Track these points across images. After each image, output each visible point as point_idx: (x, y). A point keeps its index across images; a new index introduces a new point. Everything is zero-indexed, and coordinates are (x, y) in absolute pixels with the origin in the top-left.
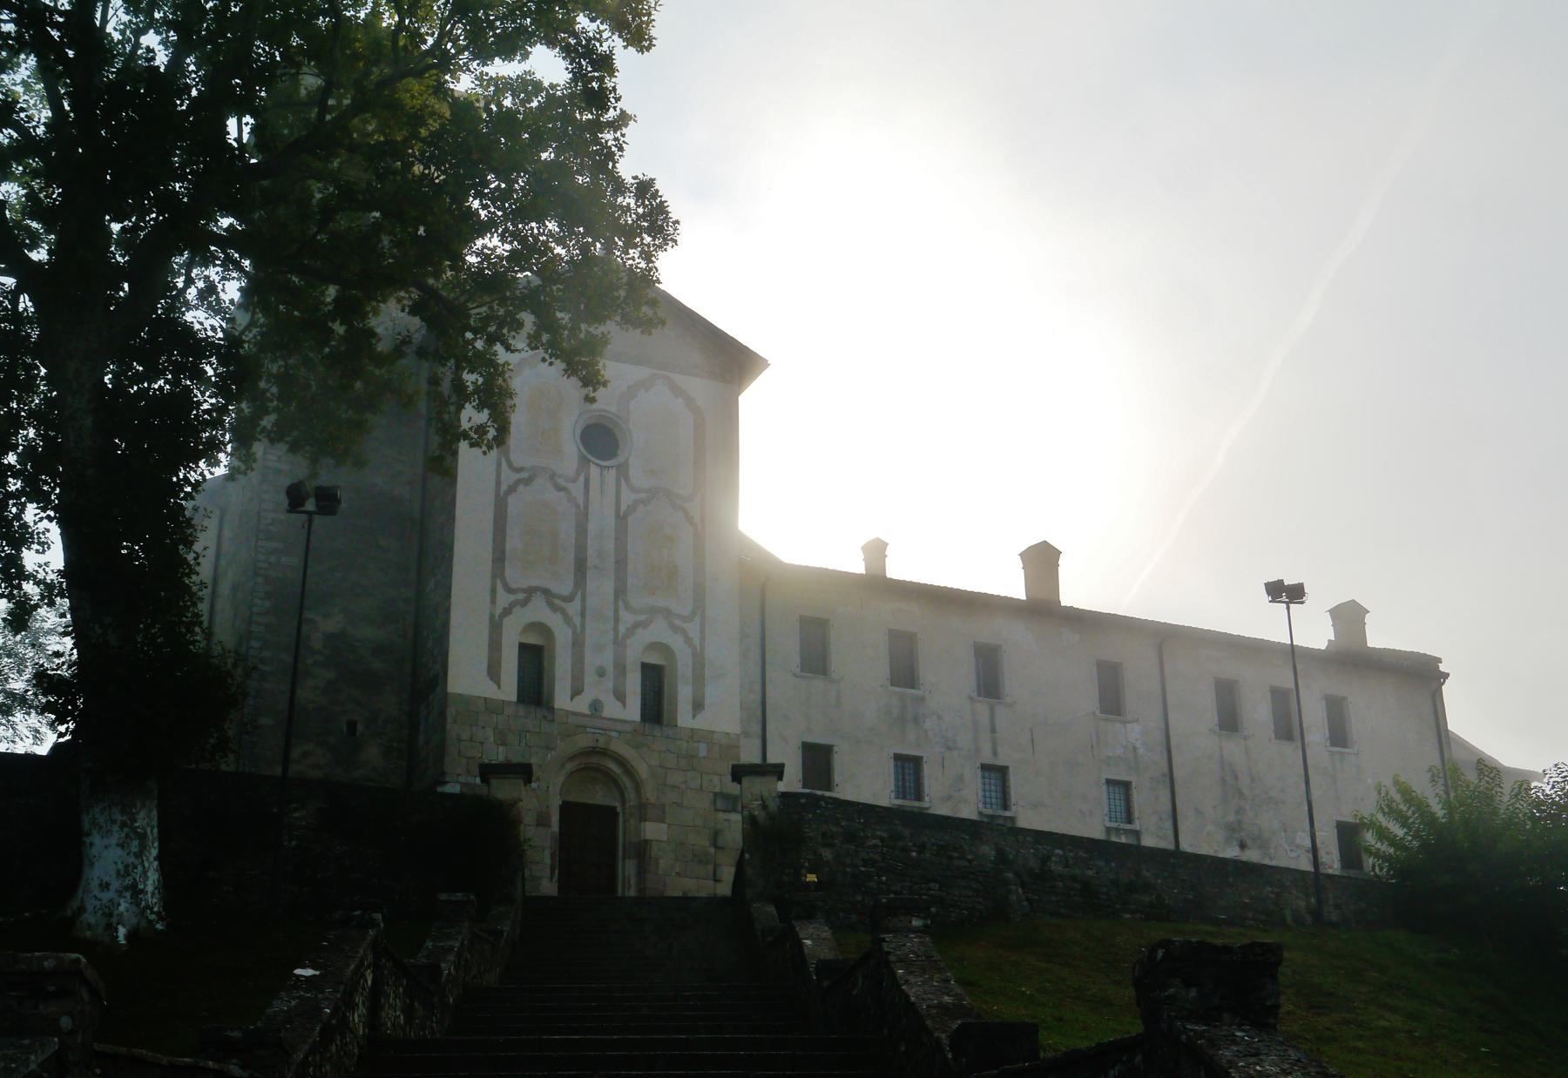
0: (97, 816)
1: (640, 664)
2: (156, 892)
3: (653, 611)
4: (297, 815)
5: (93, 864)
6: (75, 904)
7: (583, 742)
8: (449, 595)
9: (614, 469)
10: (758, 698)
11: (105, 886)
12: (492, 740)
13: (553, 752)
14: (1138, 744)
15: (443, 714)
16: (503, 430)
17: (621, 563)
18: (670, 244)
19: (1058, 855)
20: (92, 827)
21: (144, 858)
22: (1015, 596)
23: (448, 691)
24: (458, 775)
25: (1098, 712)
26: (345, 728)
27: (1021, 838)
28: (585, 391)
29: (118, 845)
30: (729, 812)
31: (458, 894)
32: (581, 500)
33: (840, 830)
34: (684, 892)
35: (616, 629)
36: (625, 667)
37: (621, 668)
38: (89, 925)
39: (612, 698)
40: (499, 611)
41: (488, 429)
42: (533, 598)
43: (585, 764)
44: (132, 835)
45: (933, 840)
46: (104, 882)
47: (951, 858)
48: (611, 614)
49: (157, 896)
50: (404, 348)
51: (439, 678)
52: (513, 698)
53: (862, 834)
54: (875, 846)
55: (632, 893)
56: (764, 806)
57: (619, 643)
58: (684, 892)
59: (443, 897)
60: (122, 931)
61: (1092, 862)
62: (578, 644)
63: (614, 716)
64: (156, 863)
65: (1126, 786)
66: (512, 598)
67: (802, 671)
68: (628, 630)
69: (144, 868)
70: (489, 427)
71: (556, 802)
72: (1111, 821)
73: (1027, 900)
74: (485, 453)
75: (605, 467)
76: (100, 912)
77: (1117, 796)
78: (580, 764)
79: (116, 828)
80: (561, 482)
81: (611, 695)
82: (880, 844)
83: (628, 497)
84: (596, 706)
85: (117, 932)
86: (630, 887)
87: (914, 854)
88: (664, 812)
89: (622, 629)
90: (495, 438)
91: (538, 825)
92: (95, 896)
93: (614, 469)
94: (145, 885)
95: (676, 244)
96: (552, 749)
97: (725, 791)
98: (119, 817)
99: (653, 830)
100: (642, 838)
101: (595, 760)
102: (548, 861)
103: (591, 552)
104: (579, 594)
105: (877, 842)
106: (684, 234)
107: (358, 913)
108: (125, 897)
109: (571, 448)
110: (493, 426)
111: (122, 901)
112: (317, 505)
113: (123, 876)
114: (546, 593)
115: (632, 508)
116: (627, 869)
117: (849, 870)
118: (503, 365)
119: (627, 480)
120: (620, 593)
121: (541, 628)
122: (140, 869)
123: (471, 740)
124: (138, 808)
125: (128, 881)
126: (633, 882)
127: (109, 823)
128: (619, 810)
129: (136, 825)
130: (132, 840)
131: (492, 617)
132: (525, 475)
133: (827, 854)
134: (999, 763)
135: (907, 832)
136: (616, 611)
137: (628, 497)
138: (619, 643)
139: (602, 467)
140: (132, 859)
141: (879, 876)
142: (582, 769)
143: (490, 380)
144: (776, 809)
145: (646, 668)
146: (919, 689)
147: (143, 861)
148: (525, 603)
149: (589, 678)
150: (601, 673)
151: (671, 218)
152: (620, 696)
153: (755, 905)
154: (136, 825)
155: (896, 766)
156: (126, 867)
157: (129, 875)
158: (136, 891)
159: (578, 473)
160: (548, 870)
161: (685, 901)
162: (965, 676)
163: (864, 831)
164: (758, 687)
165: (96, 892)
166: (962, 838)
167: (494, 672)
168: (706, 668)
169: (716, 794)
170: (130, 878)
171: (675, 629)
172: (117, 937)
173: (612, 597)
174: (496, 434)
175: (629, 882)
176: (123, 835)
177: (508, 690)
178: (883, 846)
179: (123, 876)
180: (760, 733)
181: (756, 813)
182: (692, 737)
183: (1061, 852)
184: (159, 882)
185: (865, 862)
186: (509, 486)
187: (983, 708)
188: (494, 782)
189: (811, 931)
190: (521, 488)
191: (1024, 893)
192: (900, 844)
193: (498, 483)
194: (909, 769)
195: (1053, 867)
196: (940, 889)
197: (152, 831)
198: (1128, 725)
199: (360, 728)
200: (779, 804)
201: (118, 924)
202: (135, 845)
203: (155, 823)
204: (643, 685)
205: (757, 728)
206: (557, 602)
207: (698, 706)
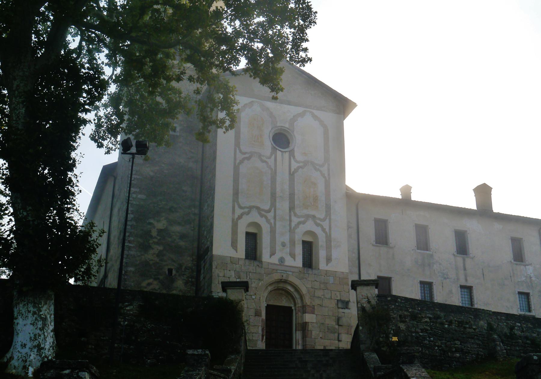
0: (21, 309)
1: (301, 242)
2: (51, 348)
3: (308, 217)
4: (128, 308)
5: (18, 334)
6: (8, 355)
7: (276, 277)
8: (213, 211)
9: (288, 152)
10: (357, 256)
11: (24, 346)
12: (234, 276)
13: (262, 282)
14: (532, 275)
15: (211, 265)
16: (233, 120)
17: (292, 196)
18: (313, 24)
19: (518, 326)
20: (18, 315)
21: (45, 331)
22: (472, 208)
23: (213, 254)
24: (218, 292)
25: (513, 261)
26: (167, 272)
27: (499, 317)
28: (273, 94)
29: (31, 324)
30: (345, 309)
31: (199, 350)
32: (273, 167)
33: (409, 314)
34: (324, 347)
35: (290, 225)
36: (295, 242)
37: (293, 243)
38: (15, 367)
39: (289, 257)
40: (236, 216)
41: (226, 120)
42: (252, 211)
43: (277, 287)
44: (38, 318)
45: (455, 319)
46: (23, 343)
47: (465, 328)
48: (288, 218)
49: (52, 351)
50: (182, 76)
51: (209, 249)
52: (244, 257)
53: (420, 316)
54: (426, 322)
55: (300, 347)
56: (369, 302)
57: (292, 231)
58: (324, 347)
59: (190, 352)
60: (31, 370)
61: (535, 330)
62: (273, 231)
63: (290, 265)
64: (52, 333)
65: (527, 295)
66: (242, 211)
67: (376, 243)
68: (295, 225)
69: (45, 336)
70: (226, 119)
71: (264, 305)
72: (521, 311)
73: (505, 349)
74: (224, 133)
75: (284, 152)
76: (21, 359)
77: (523, 299)
78: (275, 287)
79: (30, 315)
80: (264, 158)
81: (289, 254)
82: (429, 321)
83: (294, 165)
84: (282, 260)
85: (28, 370)
86: (299, 344)
87: (446, 326)
88: (314, 308)
89: (293, 225)
90: (229, 126)
91: (255, 316)
92: (18, 351)
93: (288, 152)
94: (45, 345)
95: (316, 24)
96: (262, 280)
97: (343, 299)
98: (32, 309)
99: (309, 318)
100: (304, 321)
101: (281, 285)
102: (260, 332)
103: (278, 189)
104: (273, 209)
105: (427, 320)
106: (319, 19)
107: (67, 372)
108: (34, 351)
109: (268, 143)
110: (228, 119)
111: (32, 354)
112: (137, 150)
113: (33, 340)
114: (258, 208)
115: (296, 170)
116: (297, 336)
117: (414, 334)
118: (232, 88)
119: (294, 157)
120: (292, 208)
121: (256, 225)
122: (42, 336)
123: (224, 276)
124: (42, 305)
125: (36, 343)
126: (300, 342)
127: (27, 312)
128: (293, 308)
129: (41, 313)
130: (38, 321)
131: (233, 220)
132: (247, 155)
133: (402, 326)
134: (468, 285)
135: (442, 314)
136: (290, 216)
137: (294, 165)
138: (292, 231)
139: (282, 152)
140: (38, 331)
141: (430, 338)
142: (276, 289)
143: (226, 98)
144: (375, 303)
145: (304, 242)
146: (430, 251)
147: (44, 333)
148: (248, 213)
149: (278, 247)
150: (284, 245)
151: (312, 11)
152: (293, 256)
153: (366, 354)
154: (41, 313)
155: (421, 287)
156: (35, 335)
157: (36, 340)
158: (39, 348)
159: (271, 155)
160: (261, 337)
161: (326, 352)
162: (451, 245)
163: (420, 314)
164: (356, 251)
165: (19, 349)
166: (470, 318)
167: (234, 244)
168: (332, 242)
169: (338, 300)
170: (37, 341)
171: (318, 225)
172: (28, 373)
173: (288, 211)
174: (230, 123)
175: (298, 342)
176: (34, 318)
177: (241, 253)
178: (430, 322)
179: (33, 340)
180: (358, 272)
181: (365, 305)
182: (326, 274)
183: (519, 325)
184: (53, 343)
185: (422, 331)
186: (240, 160)
187: (460, 259)
188: (229, 291)
189: (414, 372)
190: (246, 161)
191: (503, 346)
192: (439, 320)
193: (235, 159)
194: (427, 286)
195: (516, 332)
196: (460, 344)
197: (50, 317)
198: (527, 266)
199: (174, 272)
200: (376, 300)
201: (29, 366)
202: (40, 324)
203: (52, 312)
204: (304, 253)
205: (357, 270)
206: (263, 213)
207: (329, 260)
